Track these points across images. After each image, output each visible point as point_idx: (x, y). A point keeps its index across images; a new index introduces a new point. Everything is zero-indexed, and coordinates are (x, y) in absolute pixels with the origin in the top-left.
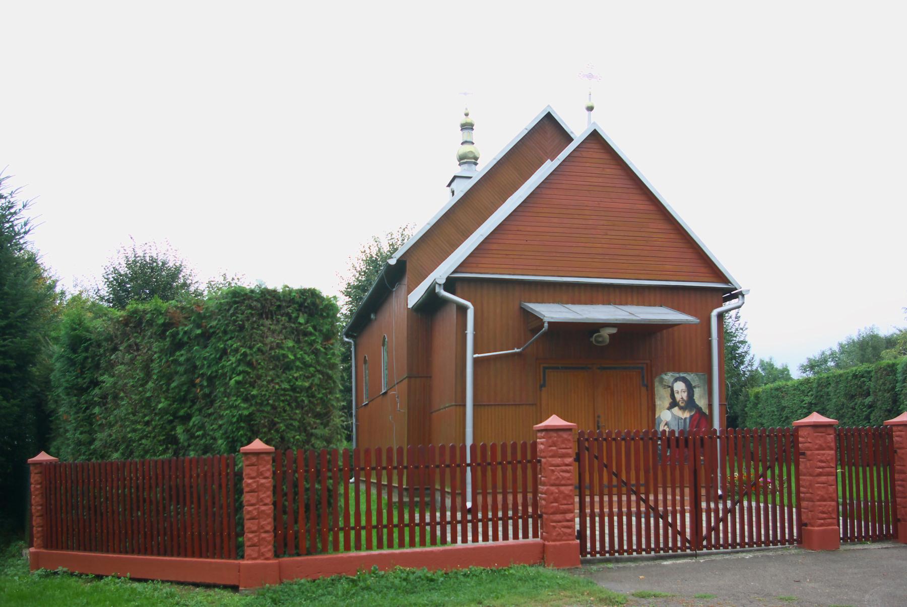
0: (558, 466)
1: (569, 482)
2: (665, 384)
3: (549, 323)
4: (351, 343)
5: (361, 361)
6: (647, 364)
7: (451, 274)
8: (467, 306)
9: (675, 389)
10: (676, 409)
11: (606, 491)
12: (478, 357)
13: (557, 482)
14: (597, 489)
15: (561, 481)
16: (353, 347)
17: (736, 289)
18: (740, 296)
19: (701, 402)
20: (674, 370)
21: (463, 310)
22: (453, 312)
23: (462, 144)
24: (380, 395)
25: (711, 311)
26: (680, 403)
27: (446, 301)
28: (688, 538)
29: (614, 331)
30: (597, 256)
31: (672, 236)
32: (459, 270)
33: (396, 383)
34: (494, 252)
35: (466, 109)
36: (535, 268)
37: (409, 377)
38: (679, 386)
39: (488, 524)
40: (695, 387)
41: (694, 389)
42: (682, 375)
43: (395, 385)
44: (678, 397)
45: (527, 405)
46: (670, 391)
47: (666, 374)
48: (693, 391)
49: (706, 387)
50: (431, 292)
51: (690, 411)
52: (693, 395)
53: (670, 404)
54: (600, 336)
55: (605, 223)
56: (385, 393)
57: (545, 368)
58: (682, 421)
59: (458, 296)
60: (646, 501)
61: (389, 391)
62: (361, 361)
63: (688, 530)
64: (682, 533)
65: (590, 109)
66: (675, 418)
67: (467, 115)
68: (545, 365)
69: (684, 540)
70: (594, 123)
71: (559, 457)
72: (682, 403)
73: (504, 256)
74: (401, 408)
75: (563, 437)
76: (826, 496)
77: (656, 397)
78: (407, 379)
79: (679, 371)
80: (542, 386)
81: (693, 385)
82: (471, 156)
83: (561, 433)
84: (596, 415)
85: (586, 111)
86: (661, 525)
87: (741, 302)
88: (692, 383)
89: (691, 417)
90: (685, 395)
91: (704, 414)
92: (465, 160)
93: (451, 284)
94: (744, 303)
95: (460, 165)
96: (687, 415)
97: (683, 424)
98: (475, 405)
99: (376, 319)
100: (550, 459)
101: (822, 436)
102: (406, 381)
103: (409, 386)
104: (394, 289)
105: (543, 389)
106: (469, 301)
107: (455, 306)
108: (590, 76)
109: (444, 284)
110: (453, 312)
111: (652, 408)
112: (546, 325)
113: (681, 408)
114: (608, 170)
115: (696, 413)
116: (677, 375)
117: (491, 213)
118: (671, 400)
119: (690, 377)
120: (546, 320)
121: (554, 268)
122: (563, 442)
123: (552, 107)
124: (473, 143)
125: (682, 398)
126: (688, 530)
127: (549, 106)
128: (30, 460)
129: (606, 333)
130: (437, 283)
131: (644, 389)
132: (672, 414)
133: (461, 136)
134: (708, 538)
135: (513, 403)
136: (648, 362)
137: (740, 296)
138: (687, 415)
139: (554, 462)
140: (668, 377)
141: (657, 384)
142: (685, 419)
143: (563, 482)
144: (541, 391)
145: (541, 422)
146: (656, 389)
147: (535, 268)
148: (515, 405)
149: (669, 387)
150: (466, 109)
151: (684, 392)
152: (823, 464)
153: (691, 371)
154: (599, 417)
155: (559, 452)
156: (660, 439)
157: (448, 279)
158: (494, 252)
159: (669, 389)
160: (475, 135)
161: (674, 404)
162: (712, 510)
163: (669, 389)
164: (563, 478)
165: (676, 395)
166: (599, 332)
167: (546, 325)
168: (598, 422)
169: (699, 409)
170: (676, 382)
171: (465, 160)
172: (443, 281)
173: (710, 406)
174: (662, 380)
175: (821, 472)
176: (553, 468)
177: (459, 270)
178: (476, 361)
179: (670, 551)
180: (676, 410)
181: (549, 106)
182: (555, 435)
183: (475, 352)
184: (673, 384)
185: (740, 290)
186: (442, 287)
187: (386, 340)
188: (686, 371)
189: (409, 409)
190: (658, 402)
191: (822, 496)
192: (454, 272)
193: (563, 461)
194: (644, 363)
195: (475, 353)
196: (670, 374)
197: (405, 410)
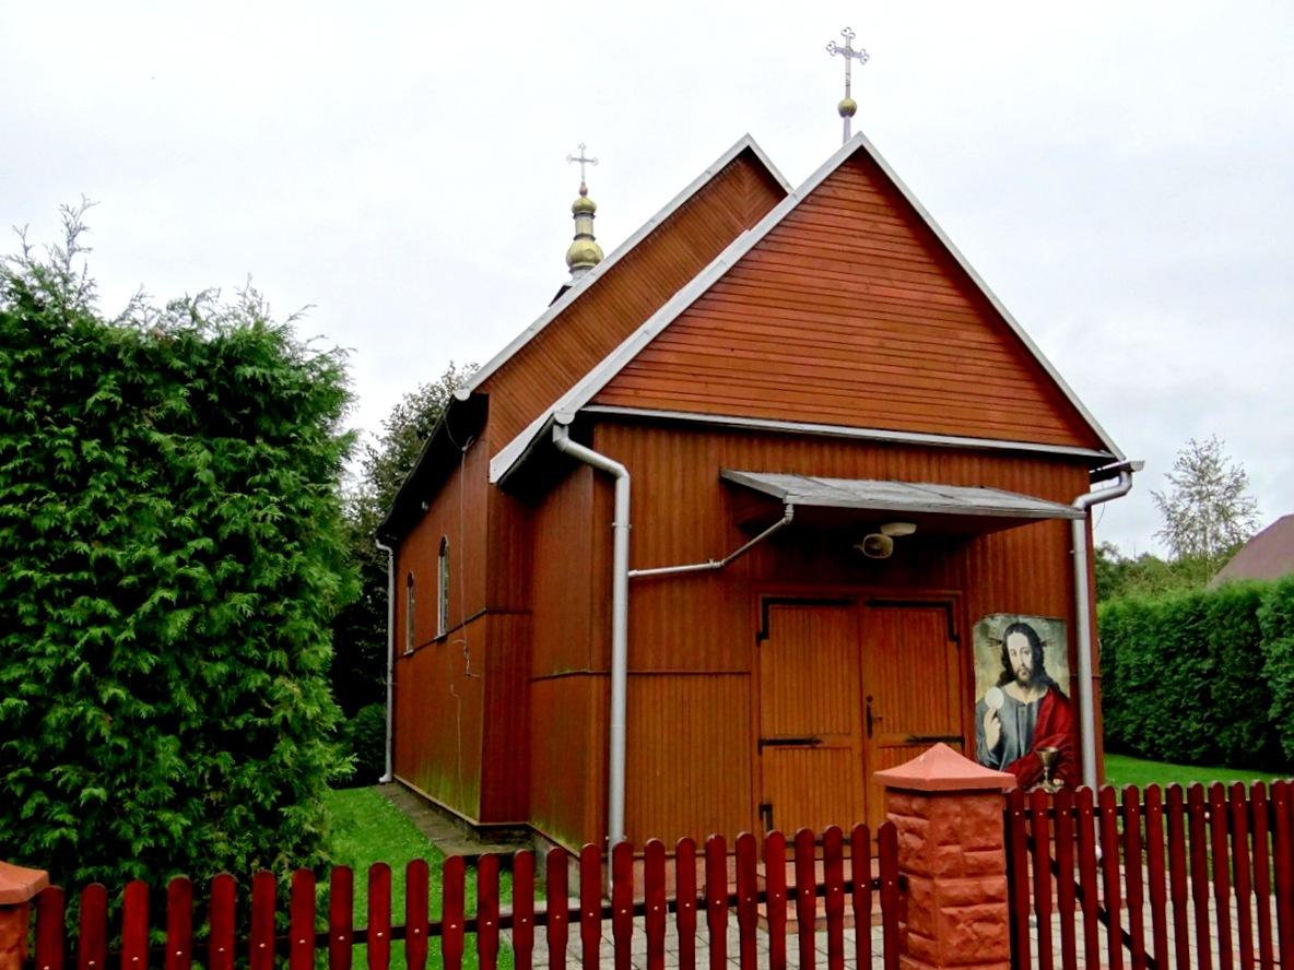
0: (967, 903)
2: (990, 636)
3: (796, 507)
4: (387, 552)
5: (403, 579)
6: (957, 596)
7: (584, 407)
8: (617, 470)
9: (1010, 647)
10: (1013, 685)
13: (966, 954)
15: (976, 951)
16: (391, 558)
17: (1115, 460)
18: (1124, 474)
21: (607, 479)
22: (586, 485)
23: (576, 238)
24: (433, 642)
26: (1020, 673)
27: (577, 462)
29: (907, 529)
30: (865, 387)
31: (1000, 357)
32: (600, 400)
33: (463, 621)
34: (670, 368)
35: (583, 184)
36: (749, 403)
37: (490, 612)
38: (1018, 642)
40: (1044, 644)
41: (1044, 649)
42: (1022, 620)
43: (461, 626)
44: (1016, 662)
45: (731, 674)
46: (1001, 651)
47: (992, 618)
48: (1042, 652)
49: (1064, 637)
50: (544, 441)
51: (1039, 689)
53: (1001, 676)
54: (875, 541)
55: (879, 324)
56: (443, 640)
57: (766, 602)
58: (1025, 709)
59: (599, 452)
61: (449, 638)
62: (403, 579)
66: (1012, 705)
67: (583, 193)
68: (768, 595)
70: (860, 134)
71: (970, 876)
72: (1024, 674)
73: (691, 377)
74: (473, 668)
75: (977, 814)
77: (976, 661)
78: (485, 616)
79: (1017, 613)
80: (763, 635)
81: (1042, 640)
82: (591, 257)
83: (973, 803)
84: (865, 696)
87: (1125, 485)
89: (1041, 701)
90: (1028, 660)
91: (1063, 696)
92: (581, 264)
93: (583, 426)
94: (1130, 486)
95: (572, 271)
96: (1033, 697)
97: (1026, 714)
98: (631, 675)
99: (428, 512)
100: (944, 883)
102: (483, 621)
103: (490, 627)
104: (464, 449)
105: (764, 642)
106: (620, 462)
107: (591, 470)
109: (570, 425)
110: (586, 485)
111: (969, 683)
112: (789, 511)
113: (1022, 684)
114: (882, 226)
115: (1048, 694)
116: (1014, 620)
117: (645, 318)
118: (1004, 669)
119: (1034, 623)
120: (790, 500)
121: (785, 406)
122: (979, 832)
123: (866, 134)
124: (593, 239)
125: (1023, 665)
127: (748, 136)
129: (887, 535)
130: (556, 423)
131: (952, 646)
133: (569, 226)
135: (702, 671)
136: (960, 592)
137: (1124, 474)
138: (1033, 697)
139: (953, 893)
140: (997, 623)
141: (976, 635)
142: (1030, 705)
143: (982, 953)
144: (759, 644)
145: (884, 769)
146: (975, 646)
147: (749, 403)
148: (710, 674)
149: (1000, 642)
150: (583, 184)
151: (1027, 653)
154: (870, 699)
155: (970, 861)
156: (1208, 807)
157: (579, 414)
158: (670, 368)
159: (1000, 646)
161: (1008, 676)
162: (1124, 903)
163: (1000, 646)
164: (982, 940)
165: (1012, 659)
166: (880, 532)
167: (789, 511)
168: (869, 709)
169: (1054, 687)
170: (1012, 632)
171: (581, 264)
172: (570, 419)
173: (1075, 681)
174: (985, 630)
176: (953, 911)
177: (600, 400)
178: (633, 584)
180: (1012, 687)
181: (748, 136)
183: (631, 567)
184: (1006, 637)
185: (1123, 462)
186: (567, 429)
187: (447, 545)
188: (1029, 614)
189: (488, 672)
190: (979, 672)
192: (589, 404)
193: (979, 886)
194: (952, 596)
196: (1000, 618)
197: (479, 675)
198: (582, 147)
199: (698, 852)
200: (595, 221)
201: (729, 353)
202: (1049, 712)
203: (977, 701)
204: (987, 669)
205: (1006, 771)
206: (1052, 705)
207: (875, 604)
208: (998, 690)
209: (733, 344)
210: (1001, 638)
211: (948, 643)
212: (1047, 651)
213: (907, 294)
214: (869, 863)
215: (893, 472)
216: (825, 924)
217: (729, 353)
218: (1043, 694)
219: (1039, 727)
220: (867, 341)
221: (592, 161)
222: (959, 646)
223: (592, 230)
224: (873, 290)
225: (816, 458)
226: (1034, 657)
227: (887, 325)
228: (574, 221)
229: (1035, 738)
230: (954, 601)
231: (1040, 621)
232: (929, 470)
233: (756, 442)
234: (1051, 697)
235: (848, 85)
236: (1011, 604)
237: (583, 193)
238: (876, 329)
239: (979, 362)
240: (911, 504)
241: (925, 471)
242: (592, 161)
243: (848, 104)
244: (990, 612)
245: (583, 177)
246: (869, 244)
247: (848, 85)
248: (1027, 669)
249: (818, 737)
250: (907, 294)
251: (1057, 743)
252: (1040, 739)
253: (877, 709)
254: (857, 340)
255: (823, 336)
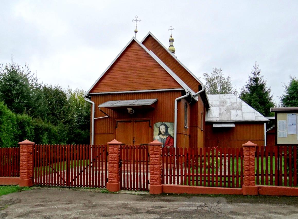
1: (158, 164)
6: (116, 120)
9: (160, 128)
10: (161, 135)
11: (136, 163)
12: (95, 119)
14: (132, 162)
19: (170, 132)
20: (161, 121)
23: (170, 46)
25: (175, 99)
28: (65, 180)
34: (102, 85)
35: (171, 35)
39: (266, 173)
41: (168, 128)
42: (164, 123)
44: (161, 131)
48: (168, 129)
51: (166, 136)
52: (168, 130)
55: (138, 71)
60: (52, 167)
63: (65, 178)
64: (63, 179)
65: (136, 32)
66: (160, 139)
67: (171, 37)
68: (117, 121)
69: (64, 182)
76: (112, 171)
77: (154, 131)
80: (116, 127)
81: (168, 127)
83: (155, 146)
85: (134, 32)
86: (62, 176)
88: (168, 126)
89: (167, 138)
90: (164, 130)
96: (165, 137)
97: (163, 140)
101: (112, 149)
108: (136, 21)
111: (152, 135)
113: (163, 135)
115: (169, 136)
116: (162, 123)
118: (159, 132)
119: (166, 123)
123: (151, 32)
125: (163, 131)
126: (65, 178)
127: (150, 32)
128: (243, 145)
131: (150, 128)
132: (159, 137)
134: (72, 182)
138: (165, 137)
140: (158, 124)
141: (154, 126)
142: (164, 139)
144: (116, 129)
146: (154, 128)
149: (158, 127)
150: (171, 35)
152: (112, 159)
153: (168, 122)
159: (158, 128)
160: (174, 43)
161: (160, 133)
163: (158, 128)
165: (161, 130)
169: (170, 136)
174: (156, 125)
175: (110, 162)
178: (95, 120)
179: (62, 185)
181: (150, 32)
182: (22, 146)
183: (95, 117)
184: (160, 126)
188: (166, 122)
190: (154, 133)
191: (111, 171)
194: (116, 121)
195: (95, 118)
196: (159, 123)
198: (171, 27)
199: (100, 161)
200: (174, 42)
201: (112, 81)
202: (168, 140)
203: (154, 138)
204: (156, 132)
205: (33, 142)
206: (169, 139)
207: (136, 121)
208: (158, 136)
209: (112, 80)
210: (159, 126)
211: (149, 128)
212: (169, 129)
213: (143, 65)
214: (121, 165)
215: (139, 98)
216: (101, 170)
217: (112, 81)
218: (167, 137)
219: (166, 143)
220: (135, 75)
221: (169, 30)
222: (151, 128)
223: (173, 44)
224: (148, 64)
225: (112, 98)
226: (166, 130)
227: (139, 71)
228: (169, 43)
229: (165, 145)
230: (116, 121)
231: (168, 123)
232: (147, 96)
233: (101, 96)
234: (169, 137)
235: (136, 27)
236: (162, 120)
237: (171, 37)
238: (137, 72)
239: (157, 75)
240: (120, 105)
241: (146, 97)
242: (169, 30)
243: (136, 30)
244: (157, 122)
245: (171, 33)
246: (137, 57)
247: (136, 27)
248: (164, 132)
249: (125, 144)
250: (143, 65)
251: (170, 146)
252: (166, 145)
253: (135, 140)
254: (134, 75)
255: (128, 75)
